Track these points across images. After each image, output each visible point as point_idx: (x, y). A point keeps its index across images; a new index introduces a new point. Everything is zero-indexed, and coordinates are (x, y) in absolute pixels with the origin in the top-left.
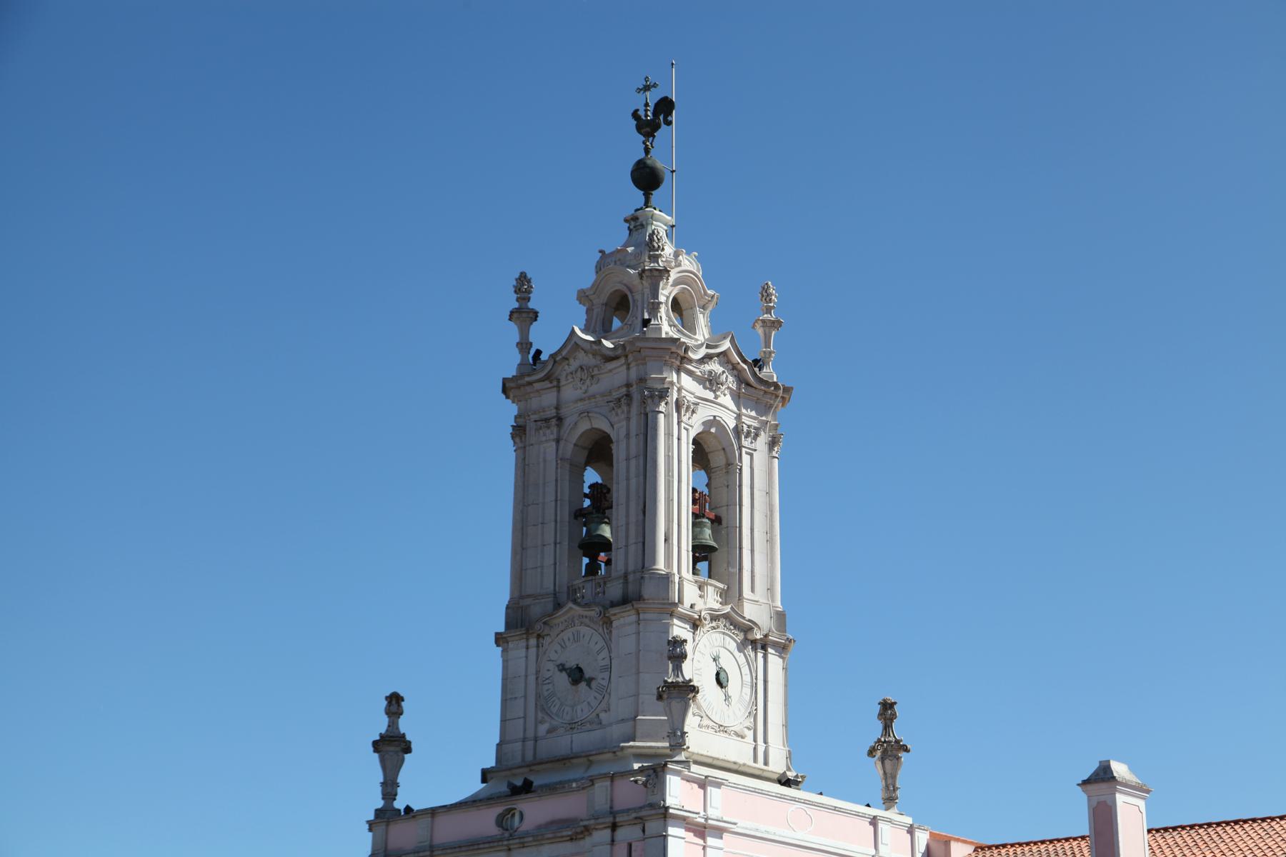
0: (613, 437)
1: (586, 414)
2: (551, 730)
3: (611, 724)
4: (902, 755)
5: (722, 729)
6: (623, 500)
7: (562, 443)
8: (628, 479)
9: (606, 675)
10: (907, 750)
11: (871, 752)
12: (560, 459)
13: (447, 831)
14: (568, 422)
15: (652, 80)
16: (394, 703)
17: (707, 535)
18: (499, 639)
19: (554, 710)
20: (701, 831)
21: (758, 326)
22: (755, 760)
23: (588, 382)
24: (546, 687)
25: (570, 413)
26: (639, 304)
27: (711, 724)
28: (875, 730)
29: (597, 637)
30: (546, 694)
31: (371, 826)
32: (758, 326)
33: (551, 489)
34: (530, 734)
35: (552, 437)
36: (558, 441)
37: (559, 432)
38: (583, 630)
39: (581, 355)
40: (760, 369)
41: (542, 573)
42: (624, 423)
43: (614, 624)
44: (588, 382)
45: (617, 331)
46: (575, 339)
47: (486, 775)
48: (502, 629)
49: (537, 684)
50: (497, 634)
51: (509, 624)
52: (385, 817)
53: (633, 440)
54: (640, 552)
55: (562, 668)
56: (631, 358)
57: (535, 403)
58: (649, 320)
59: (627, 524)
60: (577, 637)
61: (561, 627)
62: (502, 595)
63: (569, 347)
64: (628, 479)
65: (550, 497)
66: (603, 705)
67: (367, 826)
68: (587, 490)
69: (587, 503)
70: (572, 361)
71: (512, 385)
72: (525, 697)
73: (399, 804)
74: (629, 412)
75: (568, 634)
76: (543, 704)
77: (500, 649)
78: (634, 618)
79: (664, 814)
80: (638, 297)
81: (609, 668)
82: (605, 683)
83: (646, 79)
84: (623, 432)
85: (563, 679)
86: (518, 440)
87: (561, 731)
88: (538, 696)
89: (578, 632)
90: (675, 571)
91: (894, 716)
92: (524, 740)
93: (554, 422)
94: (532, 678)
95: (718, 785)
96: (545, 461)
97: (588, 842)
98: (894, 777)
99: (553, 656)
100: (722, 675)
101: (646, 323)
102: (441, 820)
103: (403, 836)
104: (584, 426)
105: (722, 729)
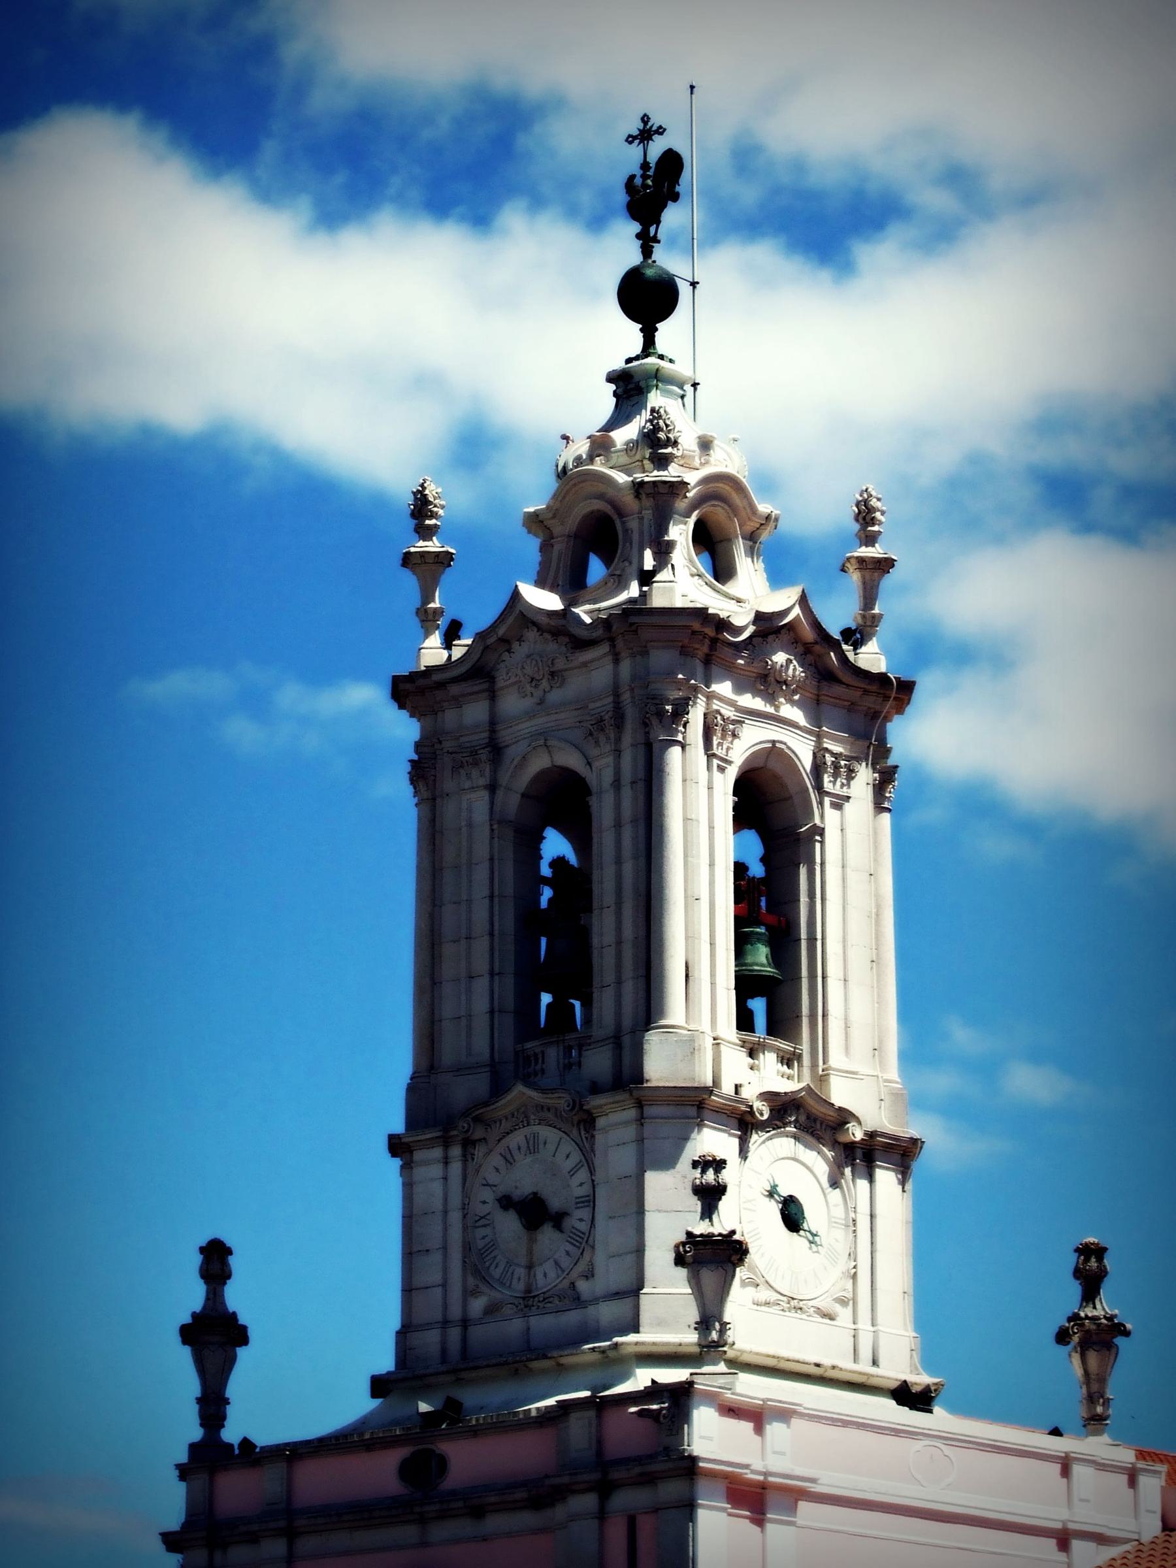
0: (591, 778)
1: (543, 739)
2: (492, 1310)
3: (596, 1300)
4: (1120, 1341)
5: (795, 1305)
6: (609, 899)
7: (500, 794)
8: (618, 861)
9: (584, 1213)
10: (1127, 1333)
11: (1062, 1337)
12: (496, 819)
13: (318, 1482)
14: (513, 753)
15: (655, 121)
16: (216, 1260)
17: (761, 955)
18: (396, 1146)
19: (497, 1273)
20: (754, 1498)
21: (851, 568)
22: (856, 1359)
23: (545, 684)
24: (482, 1232)
25: (516, 736)
26: (635, 537)
27: (774, 1297)
28: (1066, 1296)
29: (568, 1146)
30: (481, 1244)
31: (184, 1472)
32: (851, 568)
33: (481, 874)
34: (455, 1312)
35: (482, 782)
36: (492, 788)
37: (495, 771)
38: (548, 1134)
39: (531, 634)
40: (857, 645)
41: (469, 1028)
42: (610, 760)
43: (601, 1122)
44: (545, 684)
45: (598, 587)
46: (519, 608)
47: (379, 1386)
48: (399, 1127)
49: (465, 1228)
50: (391, 1138)
51: (413, 1119)
52: (210, 1458)
53: (627, 793)
54: (642, 994)
55: (506, 1202)
56: (620, 643)
57: (450, 718)
58: (653, 573)
59: (619, 943)
60: (533, 1146)
61: (506, 1126)
62: (397, 1062)
63: (510, 620)
64: (618, 861)
65: (481, 889)
66: (582, 1267)
67: (177, 1473)
68: (546, 871)
69: (547, 893)
70: (515, 646)
71: (408, 686)
72: (445, 1248)
73: (231, 1434)
74: (618, 740)
75: (517, 1139)
76: (477, 1262)
77: (397, 1162)
78: (632, 1113)
79: (689, 1467)
80: (633, 524)
81: (590, 1201)
82: (583, 1226)
83: (645, 119)
84: (608, 776)
85: (509, 1225)
86: (421, 785)
87: (508, 1310)
88: (467, 1247)
89: (535, 1136)
90: (705, 1026)
91: (1102, 1274)
92: (445, 1323)
93: (484, 755)
94: (455, 1217)
95: (785, 1414)
96: (470, 825)
97: (559, 1512)
98: (1102, 1380)
99: (493, 1178)
100: (793, 1209)
101: (646, 578)
102: (448, 1054)
103: (237, 1491)
104: (540, 763)
105: (795, 1305)
